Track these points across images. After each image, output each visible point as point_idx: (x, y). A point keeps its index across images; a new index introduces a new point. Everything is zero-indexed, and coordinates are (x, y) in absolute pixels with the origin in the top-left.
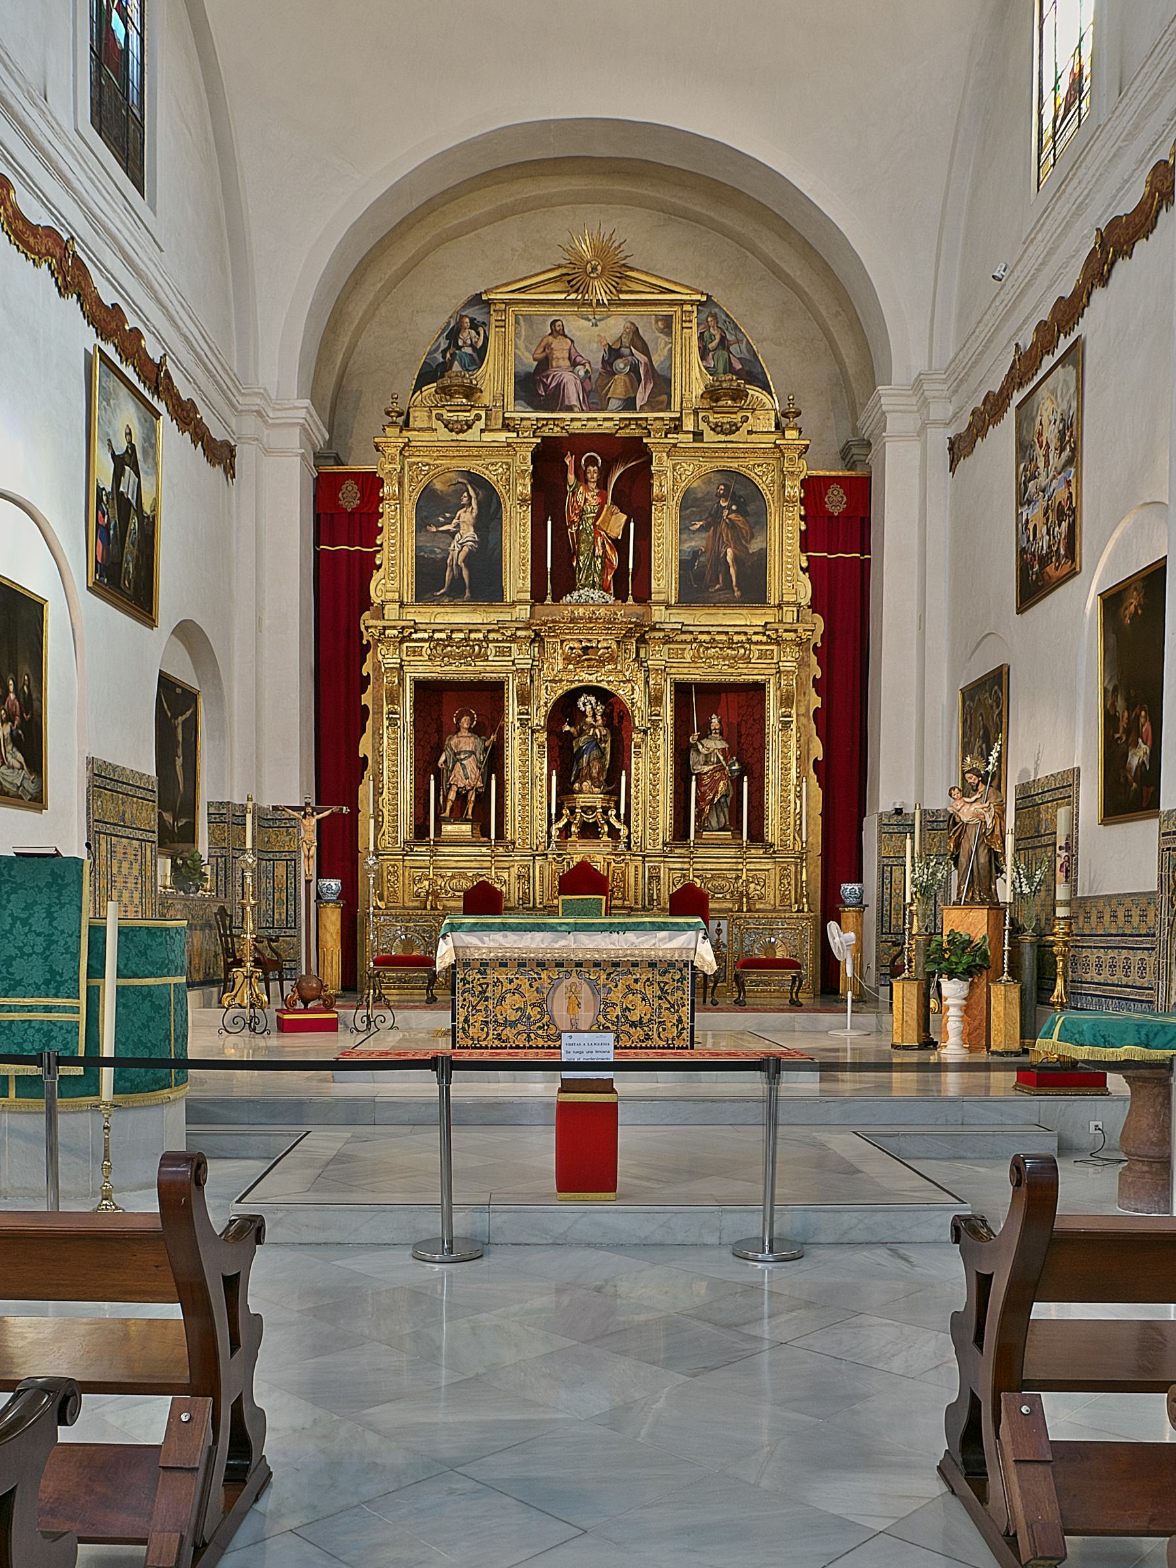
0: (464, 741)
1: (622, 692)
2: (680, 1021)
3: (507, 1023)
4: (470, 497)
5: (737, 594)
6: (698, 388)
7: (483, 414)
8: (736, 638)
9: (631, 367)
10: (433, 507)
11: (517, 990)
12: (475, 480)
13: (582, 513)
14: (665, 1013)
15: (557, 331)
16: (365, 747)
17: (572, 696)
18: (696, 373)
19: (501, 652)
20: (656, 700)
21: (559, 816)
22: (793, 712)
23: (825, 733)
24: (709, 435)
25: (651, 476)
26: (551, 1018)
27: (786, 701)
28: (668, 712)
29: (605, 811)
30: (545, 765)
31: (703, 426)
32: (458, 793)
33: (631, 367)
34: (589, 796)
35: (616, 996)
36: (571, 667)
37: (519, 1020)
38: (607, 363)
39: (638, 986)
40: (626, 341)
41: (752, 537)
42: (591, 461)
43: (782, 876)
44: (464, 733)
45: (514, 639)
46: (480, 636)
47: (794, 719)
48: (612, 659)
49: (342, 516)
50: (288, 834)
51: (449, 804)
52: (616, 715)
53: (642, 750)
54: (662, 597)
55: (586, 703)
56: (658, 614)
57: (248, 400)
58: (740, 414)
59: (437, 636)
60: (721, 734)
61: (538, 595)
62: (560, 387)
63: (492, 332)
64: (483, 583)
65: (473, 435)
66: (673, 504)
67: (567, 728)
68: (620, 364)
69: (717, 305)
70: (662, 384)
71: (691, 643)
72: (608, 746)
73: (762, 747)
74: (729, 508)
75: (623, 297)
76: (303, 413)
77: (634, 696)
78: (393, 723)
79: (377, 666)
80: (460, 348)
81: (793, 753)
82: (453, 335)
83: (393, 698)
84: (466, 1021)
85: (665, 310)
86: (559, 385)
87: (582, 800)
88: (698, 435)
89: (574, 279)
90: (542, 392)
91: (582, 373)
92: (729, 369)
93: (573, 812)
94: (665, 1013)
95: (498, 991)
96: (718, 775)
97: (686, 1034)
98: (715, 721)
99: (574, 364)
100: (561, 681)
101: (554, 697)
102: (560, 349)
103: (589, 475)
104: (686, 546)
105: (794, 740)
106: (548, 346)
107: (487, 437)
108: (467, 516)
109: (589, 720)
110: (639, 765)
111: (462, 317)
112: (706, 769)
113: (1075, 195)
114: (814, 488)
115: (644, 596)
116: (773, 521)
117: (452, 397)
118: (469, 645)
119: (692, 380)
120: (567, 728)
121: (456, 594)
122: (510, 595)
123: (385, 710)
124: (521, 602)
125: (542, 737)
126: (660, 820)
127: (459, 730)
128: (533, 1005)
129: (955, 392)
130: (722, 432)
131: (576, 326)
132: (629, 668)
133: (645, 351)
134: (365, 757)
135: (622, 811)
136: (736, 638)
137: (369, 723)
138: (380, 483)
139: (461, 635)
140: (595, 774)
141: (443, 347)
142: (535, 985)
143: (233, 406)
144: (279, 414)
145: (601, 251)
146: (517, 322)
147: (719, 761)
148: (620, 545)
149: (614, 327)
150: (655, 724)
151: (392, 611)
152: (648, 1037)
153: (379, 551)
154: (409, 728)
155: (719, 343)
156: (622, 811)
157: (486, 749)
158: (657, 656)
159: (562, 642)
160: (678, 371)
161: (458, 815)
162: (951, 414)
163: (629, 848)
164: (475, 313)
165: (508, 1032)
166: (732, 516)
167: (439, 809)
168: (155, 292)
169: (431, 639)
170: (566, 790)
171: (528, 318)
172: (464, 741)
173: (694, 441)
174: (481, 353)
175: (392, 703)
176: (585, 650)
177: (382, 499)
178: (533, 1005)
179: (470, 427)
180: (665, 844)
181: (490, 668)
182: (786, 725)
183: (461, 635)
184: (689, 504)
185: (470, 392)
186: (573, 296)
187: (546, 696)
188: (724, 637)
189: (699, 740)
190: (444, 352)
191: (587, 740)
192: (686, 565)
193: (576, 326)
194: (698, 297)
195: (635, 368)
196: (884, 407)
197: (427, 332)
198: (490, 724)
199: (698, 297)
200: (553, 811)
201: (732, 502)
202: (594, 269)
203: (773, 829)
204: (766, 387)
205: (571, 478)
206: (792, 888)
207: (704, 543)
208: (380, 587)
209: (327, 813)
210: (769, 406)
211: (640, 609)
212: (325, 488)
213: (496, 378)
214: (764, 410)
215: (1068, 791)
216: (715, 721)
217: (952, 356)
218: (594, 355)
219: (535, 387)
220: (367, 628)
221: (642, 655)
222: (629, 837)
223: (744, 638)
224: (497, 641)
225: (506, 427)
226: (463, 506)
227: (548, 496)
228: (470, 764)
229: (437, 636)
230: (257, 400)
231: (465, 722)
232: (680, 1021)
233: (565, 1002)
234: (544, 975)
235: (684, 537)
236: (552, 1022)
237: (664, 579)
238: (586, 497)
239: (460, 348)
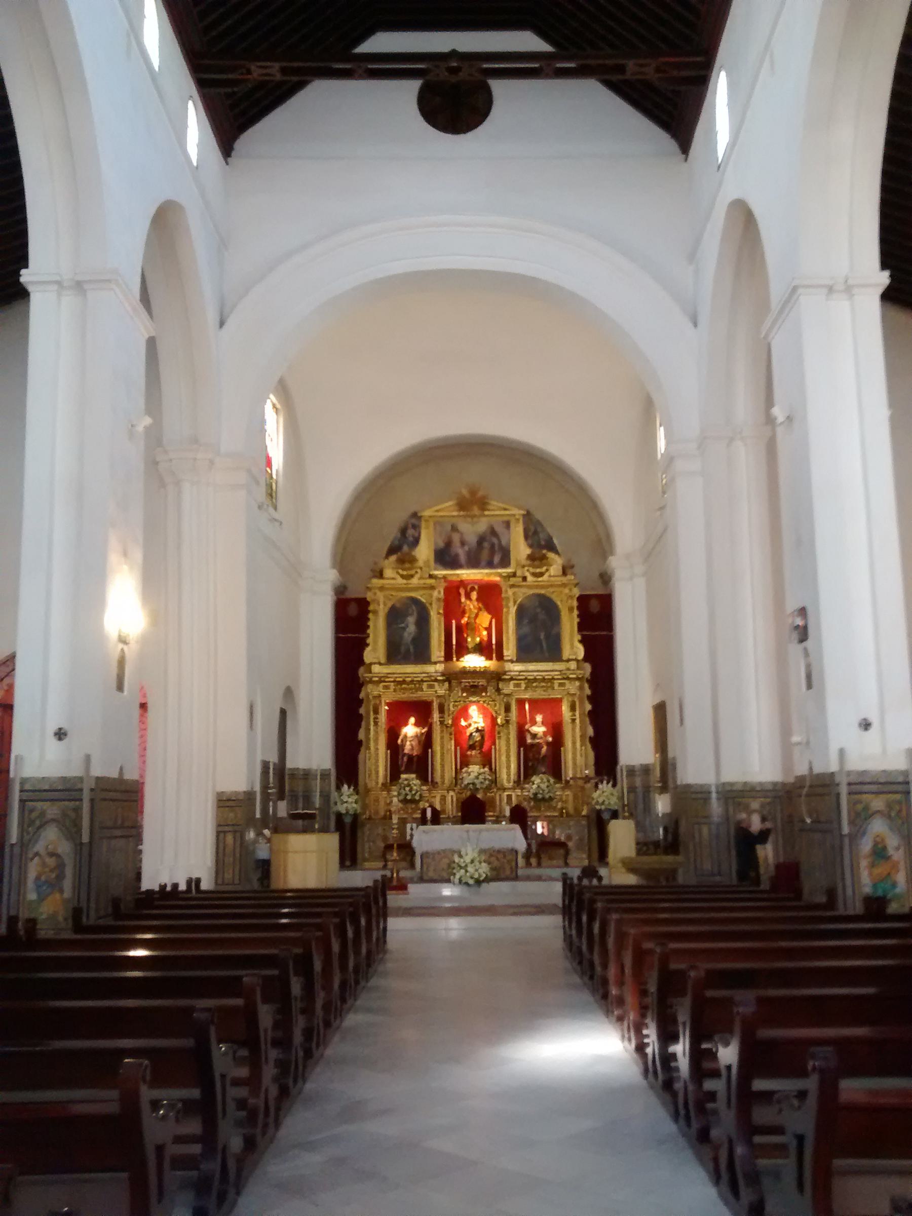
12: (415, 601)
15: (454, 528)
16: (361, 735)
23: (593, 723)
24: (530, 578)
27: (573, 708)
49: (350, 619)
56: (509, 666)
61: (448, 657)
62: (457, 555)
78: (376, 723)
79: (367, 695)
82: (403, 531)
85: (505, 519)
102: (456, 538)
108: (411, 620)
114: (583, 600)
119: (521, 550)
121: (406, 659)
122: (434, 658)
149: (482, 526)
164: (414, 521)
181: (426, 693)
184: (521, 612)
185: (413, 560)
195: (493, 546)
197: (391, 534)
203: (569, 773)
204: (557, 553)
208: (369, 655)
211: (499, 663)
213: (424, 551)
214: (556, 562)
218: (472, 539)
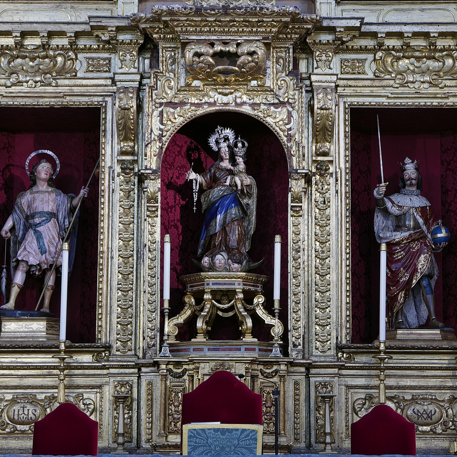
1: (275, 119)
17: (197, 131)
20: (322, 132)
29: (249, 298)
34: (224, 273)
44: (43, 186)
51: (15, 291)
71: (374, 51)
72: (252, 203)
90: (190, 152)
93: (199, 300)
96: (416, 246)
98: (410, 169)
110: (301, 227)
127: (33, 182)
135: (277, 295)
147: (417, 226)
150: (322, 169)
156: (277, 295)
157: (72, 210)
158: (326, 70)
163: (285, 353)
180: (339, 348)
181: (79, 87)
187: (160, 126)
189: (388, 194)
198: (79, 174)
216: (410, 169)
222: (285, 337)
224: (90, 49)
228: (49, 230)
231: (44, 169)
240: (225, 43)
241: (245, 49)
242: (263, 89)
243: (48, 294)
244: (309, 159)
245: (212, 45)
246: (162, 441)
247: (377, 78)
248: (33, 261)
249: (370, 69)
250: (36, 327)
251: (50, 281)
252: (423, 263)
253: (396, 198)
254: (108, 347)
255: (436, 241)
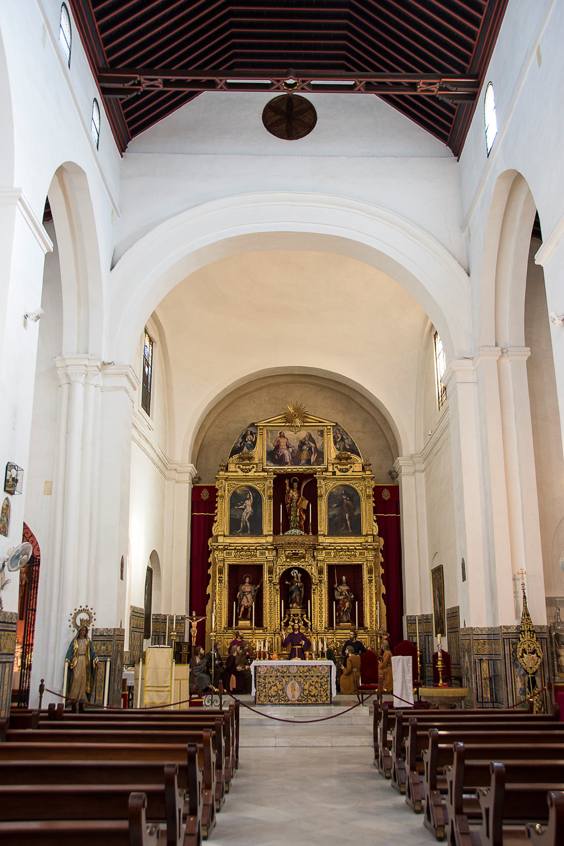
0: (247, 588)
1: (308, 569)
2: (327, 695)
3: (272, 696)
4: (250, 496)
5: (350, 531)
6: (333, 455)
7: (255, 466)
8: (350, 548)
9: (309, 449)
10: (236, 500)
11: (275, 685)
13: (292, 500)
14: (322, 692)
15: (282, 436)
16: (209, 590)
17: (288, 571)
18: (332, 450)
19: (262, 554)
20: (320, 572)
21: (284, 619)
22: (373, 576)
24: (338, 473)
25: (317, 488)
26: (286, 694)
27: (370, 572)
28: (325, 577)
29: (302, 615)
30: (279, 598)
31: (336, 470)
32: (244, 608)
33: (309, 449)
34: (296, 610)
35: (306, 687)
36: (288, 560)
37: (276, 695)
38: (300, 447)
39: (314, 683)
40: (307, 439)
41: (355, 510)
42: (295, 481)
43: (371, 641)
44: (247, 584)
45: (267, 549)
46: (254, 548)
47: (374, 578)
48: (304, 557)
50: (181, 626)
51: (241, 613)
52: (306, 577)
53: (316, 592)
54: (322, 533)
55: (294, 573)
57: (172, 466)
58: (349, 465)
59: (237, 548)
60: (346, 583)
61: (276, 532)
62: (283, 455)
63: (258, 436)
64: (255, 529)
65: (251, 474)
66: (325, 497)
67: (287, 583)
68: (305, 447)
69: (340, 426)
70: (320, 454)
71: (333, 550)
72: (303, 590)
73: (362, 589)
74: (346, 499)
75: (305, 424)
76: (191, 468)
77: (313, 571)
78: (220, 582)
79: (214, 559)
80: (246, 442)
81: (374, 592)
82: (244, 437)
83: (221, 572)
84: (259, 695)
86: (283, 455)
87: (293, 611)
88: (334, 473)
89: (288, 419)
90: (276, 457)
91: (291, 450)
92: (345, 449)
93: (289, 616)
94: (322, 692)
95: (269, 685)
96: (345, 600)
97: (329, 699)
98: (344, 578)
99: (288, 447)
100: (285, 565)
101: (282, 571)
102: (283, 442)
103: (294, 490)
104: (331, 513)
105: (374, 586)
106: (279, 441)
107: (257, 474)
108: (249, 503)
109: (295, 579)
110: (315, 597)
111: (247, 431)
112: (341, 598)
113: (445, 423)
114: (378, 491)
115: (315, 532)
116: (363, 504)
117: (244, 460)
118: (250, 550)
119: (331, 452)
120: (287, 583)
121: (245, 532)
122: (265, 532)
123: (217, 576)
124: (270, 535)
125: (278, 587)
126: (324, 619)
127: (245, 583)
128: (280, 690)
129: (424, 461)
130: (343, 472)
131: (289, 434)
132: (311, 561)
133: (314, 442)
134: (209, 594)
135: (309, 616)
136: (350, 548)
137: (211, 581)
138: (217, 490)
139: (247, 548)
140: (298, 601)
141: (240, 441)
142: (281, 683)
143: (167, 468)
144: (182, 469)
145: (297, 409)
146: (267, 433)
147: (346, 594)
148: (306, 512)
149: (303, 434)
150: (321, 581)
151: (221, 539)
152: (317, 700)
153: (216, 515)
154: (226, 583)
155: (341, 439)
156: (309, 616)
157: (255, 590)
158: (321, 556)
159: (285, 551)
160: (326, 450)
161: (245, 618)
162: (423, 468)
163: (312, 630)
165: (273, 699)
166: (348, 502)
167: (237, 615)
168: (151, 445)
169: (235, 549)
170: (287, 607)
171: (271, 431)
172: (247, 588)
173: (333, 475)
174: (254, 444)
175: (221, 574)
176: (294, 554)
177: (217, 497)
178: (280, 690)
179: (250, 471)
180: (325, 628)
181: (258, 559)
182: (370, 581)
183: (247, 548)
184: (331, 497)
185: (251, 458)
186: (287, 424)
187: (279, 571)
188: (346, 548)
189: (338, 586)
190: (241, 443)
191: (295, 588)
192: (331, 520)
193: (289, 434)
194: (332, 424)
195: (310, 449)
196: (400, 462)
198: (257, 580)
199: (332, 424)
200: (283, 616)
201: (346, 500)
202: (295, 416)
205: (288, 488)
206: (375, 646)
207: (337, 512)
208: (216, 529)
209: (201, 620)
210: (360, 462)
212: (196, 492)
213: (259, 453)
215: (455, 614)
216: (344, 578)
217: (423, 448)
218: (295, 444)
219: (274, 456)
220: (211, 546)
221: (315, 554)
222: (311, 626)
223: (353, 548)
224: (260, 549)
225: (264, 470)
226: (248, 499)
227: (279, 496)
228: (249, 596)
229: (237, 548)
230: (176, 466)
231: (247, 580)
232: (327, 695)
233: (291, 689)
234: (284, 680)
235: (330, 510)
236: (286, 696)
237: (323, 527)
238: (294, 494)
239: (246, 442)
240: (295, 551)
241: (300, 552)
242: (305, 561)
243: (249, 613)
244: (317, 579)
245: (292, 551)
246: (281, 653)
247: (335, 557)
248: (246, 605)
249: (332, 554)
250: (248, 622)
251: (250, 609)
252: (347, 604)
253: (341, 587)
254: (266, 628)
255: (351, 598)
